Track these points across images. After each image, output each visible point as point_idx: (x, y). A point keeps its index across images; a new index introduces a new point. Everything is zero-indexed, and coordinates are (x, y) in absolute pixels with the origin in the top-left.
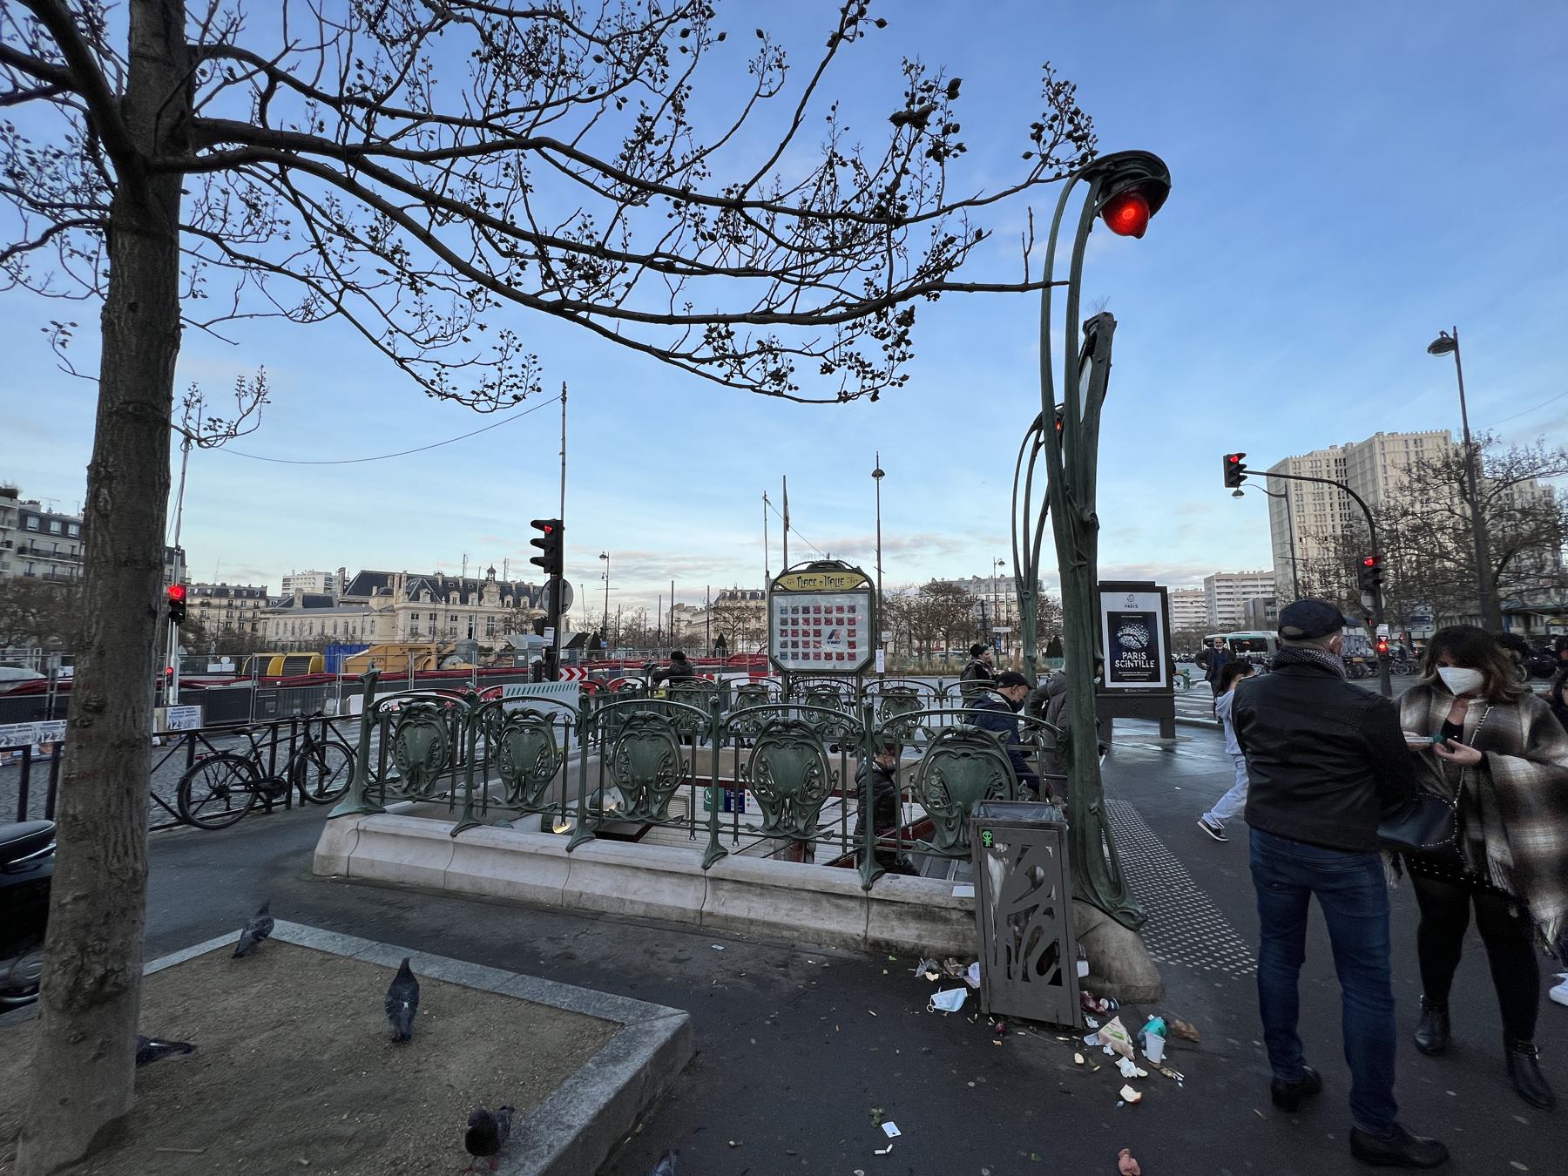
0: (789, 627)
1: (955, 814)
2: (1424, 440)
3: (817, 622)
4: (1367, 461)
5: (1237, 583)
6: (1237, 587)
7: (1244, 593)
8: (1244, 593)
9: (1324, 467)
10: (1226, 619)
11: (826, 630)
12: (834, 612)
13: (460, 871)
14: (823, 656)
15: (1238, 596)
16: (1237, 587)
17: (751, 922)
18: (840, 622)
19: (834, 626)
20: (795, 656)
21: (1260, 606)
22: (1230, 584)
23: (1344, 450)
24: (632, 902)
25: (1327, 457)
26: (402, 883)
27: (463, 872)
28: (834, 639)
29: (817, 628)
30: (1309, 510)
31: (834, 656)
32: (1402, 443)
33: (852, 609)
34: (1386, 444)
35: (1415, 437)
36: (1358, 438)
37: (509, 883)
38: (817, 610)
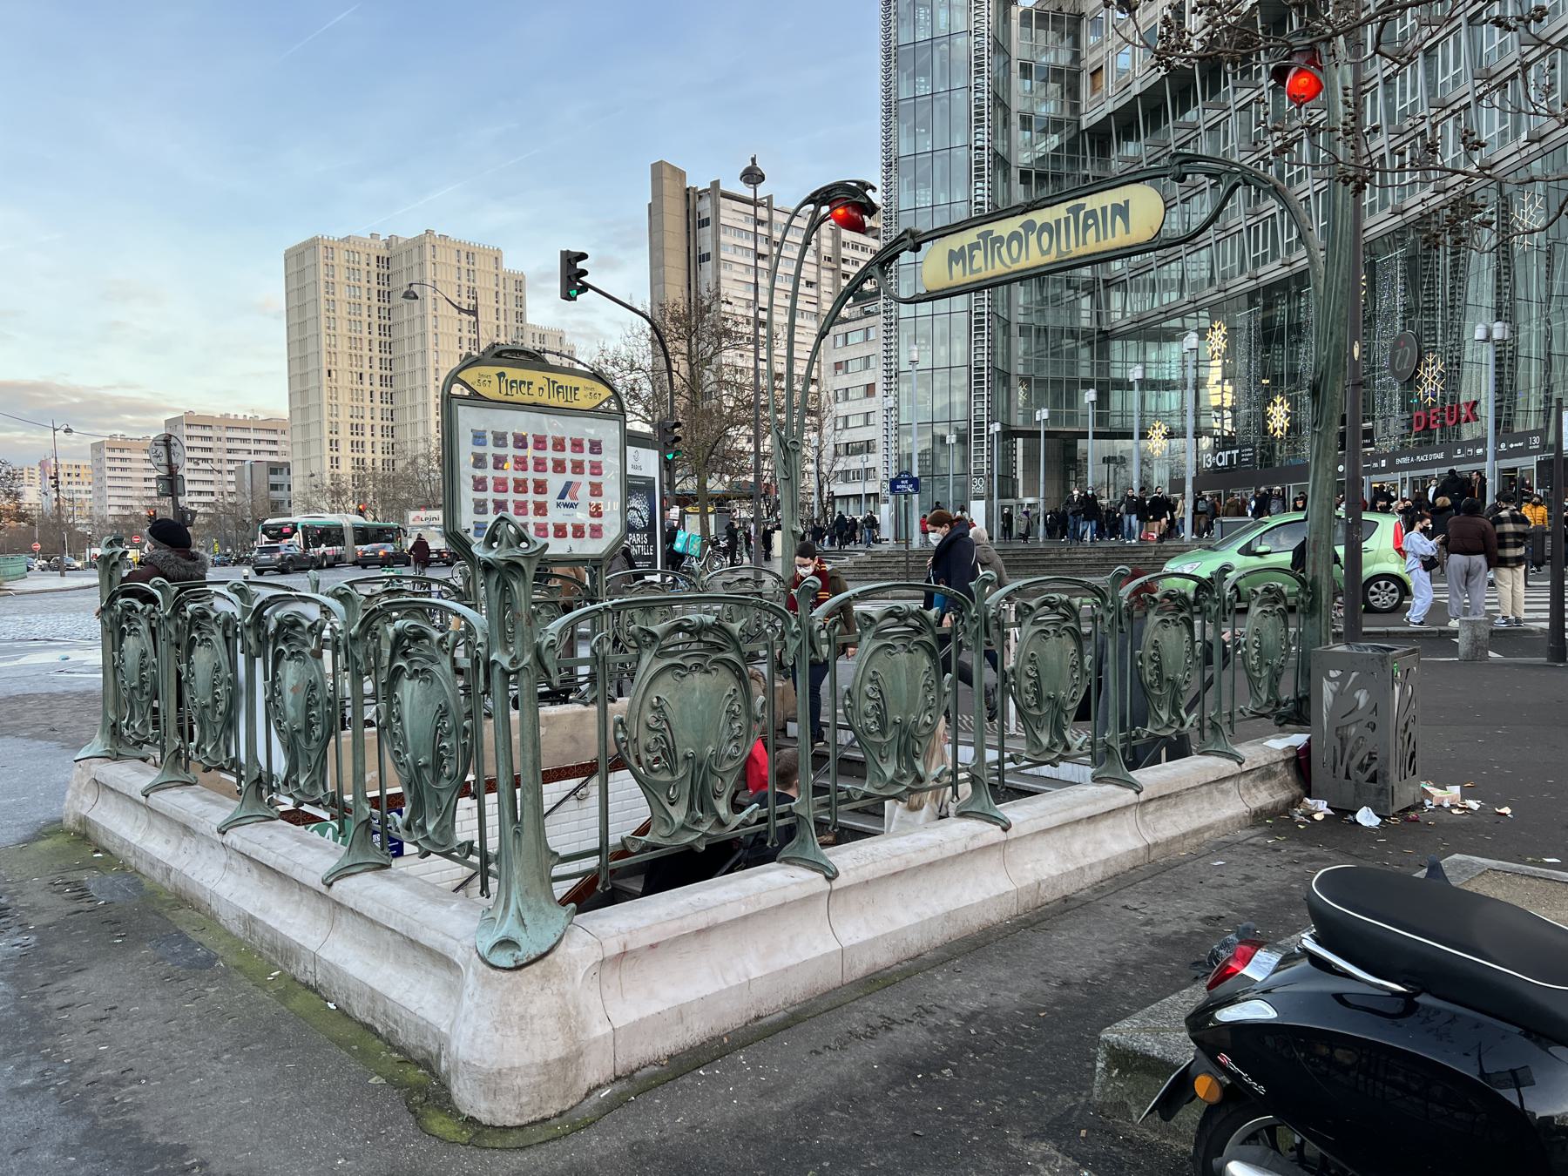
0: (489, 473)
1: (681, 774)
2: (477, 256)
3: (540, 465)
4: (416, 269)
5: (219, 434)
6: (219, 439)
7: (229, 451)
8: (229, 451)
10: (200, 493)
11: (555, 482)
13: (864, 936)
15: (219, 455)
16: (219, 439)
17: (1184, 835)
18: (578, 467)
19: (569, 476)
21: (262, 472)
22: (207, 433)
24: (1091, 866)
25: (368, 251)
26: (758, 1018)
27: (871, 936)
28: (568, 500)
29: (540, 476)
30: (343, 328)
31: (570, 529)
32: (454, 253)
33: (479, 438)
34: (437, 249)
35: (467, 249)
36: (408, 230)
37: (948, 916)
38: (540, 443)
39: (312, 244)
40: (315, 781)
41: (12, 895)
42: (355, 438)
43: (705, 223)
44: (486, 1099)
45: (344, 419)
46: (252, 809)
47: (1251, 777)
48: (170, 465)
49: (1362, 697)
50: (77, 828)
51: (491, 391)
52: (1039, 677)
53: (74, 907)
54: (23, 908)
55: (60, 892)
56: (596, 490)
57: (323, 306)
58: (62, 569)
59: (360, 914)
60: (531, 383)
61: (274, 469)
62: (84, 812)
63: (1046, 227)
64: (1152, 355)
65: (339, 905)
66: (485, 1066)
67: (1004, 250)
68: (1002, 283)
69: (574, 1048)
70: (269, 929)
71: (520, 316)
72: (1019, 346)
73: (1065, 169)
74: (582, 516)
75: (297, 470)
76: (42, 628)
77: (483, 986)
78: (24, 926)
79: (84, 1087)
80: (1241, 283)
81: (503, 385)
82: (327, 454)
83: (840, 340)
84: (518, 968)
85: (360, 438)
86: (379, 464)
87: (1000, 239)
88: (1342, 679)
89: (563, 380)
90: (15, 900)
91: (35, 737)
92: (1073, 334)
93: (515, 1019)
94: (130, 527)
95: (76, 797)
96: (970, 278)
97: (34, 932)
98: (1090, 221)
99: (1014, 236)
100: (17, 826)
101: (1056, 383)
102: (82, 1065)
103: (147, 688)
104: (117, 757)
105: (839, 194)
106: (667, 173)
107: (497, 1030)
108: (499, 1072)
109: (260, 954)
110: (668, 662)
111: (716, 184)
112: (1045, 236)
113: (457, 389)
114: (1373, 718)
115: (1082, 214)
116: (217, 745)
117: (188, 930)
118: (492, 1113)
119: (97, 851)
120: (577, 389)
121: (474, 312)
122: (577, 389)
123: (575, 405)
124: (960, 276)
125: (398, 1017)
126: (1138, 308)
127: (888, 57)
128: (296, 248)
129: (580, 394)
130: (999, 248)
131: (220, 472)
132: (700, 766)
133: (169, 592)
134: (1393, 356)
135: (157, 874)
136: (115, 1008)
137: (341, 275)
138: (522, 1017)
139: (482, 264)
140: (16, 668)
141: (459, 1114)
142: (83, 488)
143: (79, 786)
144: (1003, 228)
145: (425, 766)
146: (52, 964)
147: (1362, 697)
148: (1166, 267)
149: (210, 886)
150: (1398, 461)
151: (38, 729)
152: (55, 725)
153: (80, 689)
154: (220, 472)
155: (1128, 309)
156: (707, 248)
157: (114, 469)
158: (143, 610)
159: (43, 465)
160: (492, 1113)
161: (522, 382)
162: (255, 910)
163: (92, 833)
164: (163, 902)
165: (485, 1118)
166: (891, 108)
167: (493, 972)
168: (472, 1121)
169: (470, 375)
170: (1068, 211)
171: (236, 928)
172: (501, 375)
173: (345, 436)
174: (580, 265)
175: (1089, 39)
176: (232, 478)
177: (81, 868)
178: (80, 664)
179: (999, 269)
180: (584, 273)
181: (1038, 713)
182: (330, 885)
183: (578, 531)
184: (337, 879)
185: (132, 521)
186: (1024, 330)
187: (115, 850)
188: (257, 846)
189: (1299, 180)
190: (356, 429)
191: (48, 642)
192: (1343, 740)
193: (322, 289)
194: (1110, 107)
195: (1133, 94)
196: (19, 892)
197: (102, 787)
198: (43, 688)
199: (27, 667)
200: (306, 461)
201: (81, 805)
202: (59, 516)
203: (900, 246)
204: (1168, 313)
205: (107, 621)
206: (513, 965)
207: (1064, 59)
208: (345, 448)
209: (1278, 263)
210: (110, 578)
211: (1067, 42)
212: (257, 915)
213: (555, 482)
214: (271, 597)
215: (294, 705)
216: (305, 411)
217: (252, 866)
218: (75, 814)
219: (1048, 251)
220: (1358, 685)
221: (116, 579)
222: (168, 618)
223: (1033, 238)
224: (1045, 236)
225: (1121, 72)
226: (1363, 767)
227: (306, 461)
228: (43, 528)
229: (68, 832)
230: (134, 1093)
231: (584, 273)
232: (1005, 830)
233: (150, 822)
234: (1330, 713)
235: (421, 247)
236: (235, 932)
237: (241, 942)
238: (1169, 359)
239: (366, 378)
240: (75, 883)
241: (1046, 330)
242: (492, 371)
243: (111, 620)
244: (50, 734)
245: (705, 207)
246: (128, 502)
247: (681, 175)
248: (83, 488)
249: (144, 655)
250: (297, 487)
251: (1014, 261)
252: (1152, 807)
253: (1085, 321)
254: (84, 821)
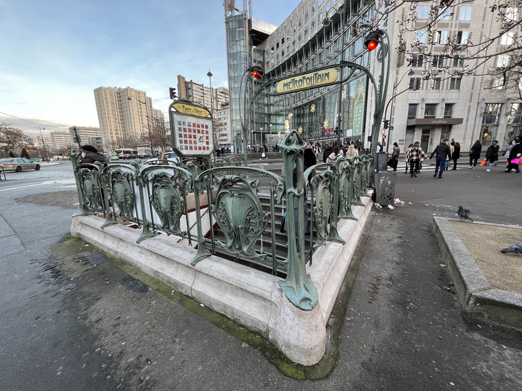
5: (83, 131)
6: (83, 132)
7: (86, 135)
8: (86, 135)
9: (113, 94)
12: (201, 127)
14: (198, 148)
16: (83, 132)
20: (186, 148)
21: (95, 140)
23: (119, 90)
28: (201, 140)
29: (194, 134)
30: (110, 108)
31: (202, 148)
36: (124, 87)
39: (100, 88)
40: (176, 228)
41: (60, 265)
43: (190, 89)
44: (306, 358)
45: (113, 127)
46: (147, 234)
48: (76, 135)
49: (389, 182)
50: (77, 236)
51: (181, 110)
53: (86, 268)
54: (66, 271)
55: (78, 262)
56: (207, 138)
57: (105, 103)
58: (48, 161)
59: (213, 277)
61: (97, 139)
62: (78, 232)
63: (308, 78)
65: (197, 271)
66: (306, 347)
67: (298, 84)
70: (166, 276)
71: (151, 107)
72: (255, 116)
73: (262, 82)
74: (204, 144)
75: (103, 139)
76: (46, 175)
77: (299, 317)
78: (69, 279)
79: (123, 373)
80: (294, 106)
82: (110, 135)
83: (219, 114)
86: (122, 138)
87: (297, 81)
88: (385, 179)
89: (198, 109)
90: (62, 267)
91: (52, 205)
92: (264, 114)
93: (314, 328)
94: (63, 152)
95: (75, 227)
96: (289, 90)
97: (73, 282)
98: (319, 77)
99: (301, 80)
100: (55, 236)
101: (262, 123)
102: (118, 357)
103: (96, 196)
104: (87, 215)
105: (256, 69)
106: (181, 78)
107: (308, 333)
108: (311, 349)
109: (163, 283)
111: (191, 81)
112: (308, 80)
113: (173, 109)
114: (392, 186)
115: (317, 75)
116: (128, 214)
117: (132, 274)
118: (308, 362)
119: (86, 244)
121: (145, 103)
123: (201, 116)
124: (286, 90)
127: (228, 55)
128: (97, 89)
129: (202, 113)
133: (101, 166)
134: (320, 120)
135: (112, 253)
136: (119, 318)
137: (108, 96)
138: (316, 326)
139: (141, 95)
140: (41, 186)
141: (292, 362)
142: (50, 143)
143: (75, 224)
144: (298, 78)
146: (85, 297)
147: (389, 182)
149: (136, 259)
151: (53, 203)
152: (58, 201)
153: (62, 191)
156: (191, 94)
158: (91, 172)
159: (38, 137)
160: (308, 362)
162: (158, 269)
163: (82, 238)
164: (117, 263)
165: (305, 364)
166: (229, 66)
167: (303, 312)
168: (299, 366)
169: (176, 106)
171: (151, 274)
172: (183, 106)
173: (114, 131)
174: (174, 91)
175: (266, 56)
176: (88, 141)
177: (83, 251)
178: (60, 184)
179: (296, 88)
183: (204, 148)
185: (64, 150)
186: (256, 113)
187: (93, 244)
188: (155, 248)
190: (116, 130)
191: (49, 178)
192: (384, 191)
193: (104, 99)
194: (270, 70)
196: (63, 263)
197: (83, 224)
198: (52, 191)
199: (45, 185)
200: (105, 137)
201: (75, 229)
202: (45, 149)
204: (281, 111)
205: (77, 175)
207: (262, 60)
208: (114, 135)
209: (306, 100)
210: (76, 162)
211: (262, 56)
212: (159, 270)
213: (198, 136)
214: (150, 167)
215: (165, 203)
216: (103, 126)
218: (75, 232)
219: (309, 84)
220: (388, 180)
221: (78, 163)
222: (102, 174)
223: (305, 81)
224: (308, 80)
225: (272, 63)
226: (388, 197)
227: (105, 137)
228: (41, 152)
229: (73, 237)
230: (148, 372)
233: (105, 236)
234: (381, 186)
235: (127, 91)
236: (150, 274)
237: (153, 278)
238: (280, 120)
239: (117, 119)
240: (83, 257)
242: (181, 105)
243: (78, 175)
244: (57, 204)
245: (189, 85)
246: (62, 146)
247: (184, 78)
248: (50, 143)
249: (93, 186)
250: (104, 143)
251: (300, 86)
253: (266, 111)
254: (79, 234)
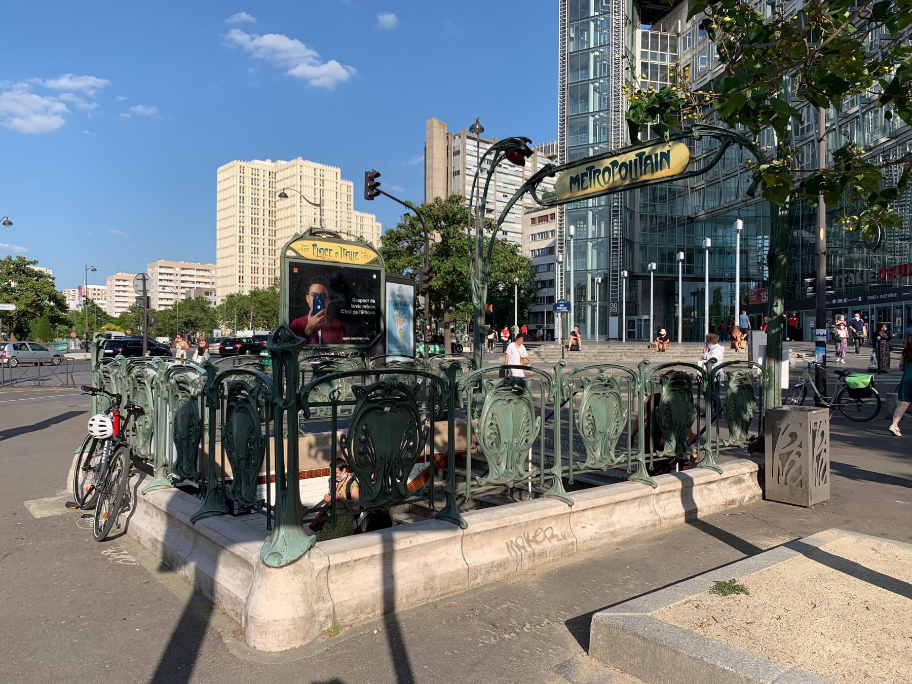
7: (183, 282)
8: (183, 282)
42: (253, 275)
47: (728, 481)
52: (594, 420)
60: (331, 250)
63: (624, 164)
64: (720, 233)
67: (601, 177)
68: (584, 199)
69: (310, 612)
81: (316, 251)
84: (281, 567)
85: (256, 275)
98: (649, 162)
110: (371, 405)
120: (357, 253)
122: (357, 253)
125: (223, 594)
126: (711, 205)
130: (598, 176)
131: (176, 294)
132: (389, 463)
145: (242, 459)
148: (728, 181)
150: (869, 298)
154: (176, 294)
155: (706, 204)
157: (119, 291)
161: (326, 249)
169: (297, 246)
170: (637, 155)
172: (314, 245)
174: (376, 180)
180: (378, 184)
181: (594, 440)
182: (194, 523)
184: (198, 519)
189: (808, 130)
195: (708, 80)
203: (543, 174)
206: (278, 565)
217: (158, 512)
231: (378, 184)
232: (570, 506)
241: (656, 217)
242: (309, 243)
252: (664, 496)
